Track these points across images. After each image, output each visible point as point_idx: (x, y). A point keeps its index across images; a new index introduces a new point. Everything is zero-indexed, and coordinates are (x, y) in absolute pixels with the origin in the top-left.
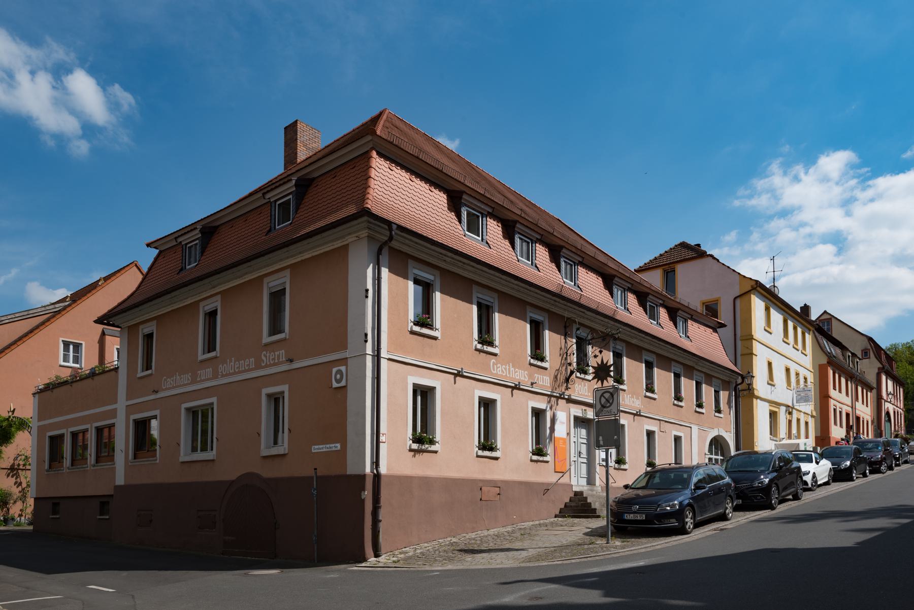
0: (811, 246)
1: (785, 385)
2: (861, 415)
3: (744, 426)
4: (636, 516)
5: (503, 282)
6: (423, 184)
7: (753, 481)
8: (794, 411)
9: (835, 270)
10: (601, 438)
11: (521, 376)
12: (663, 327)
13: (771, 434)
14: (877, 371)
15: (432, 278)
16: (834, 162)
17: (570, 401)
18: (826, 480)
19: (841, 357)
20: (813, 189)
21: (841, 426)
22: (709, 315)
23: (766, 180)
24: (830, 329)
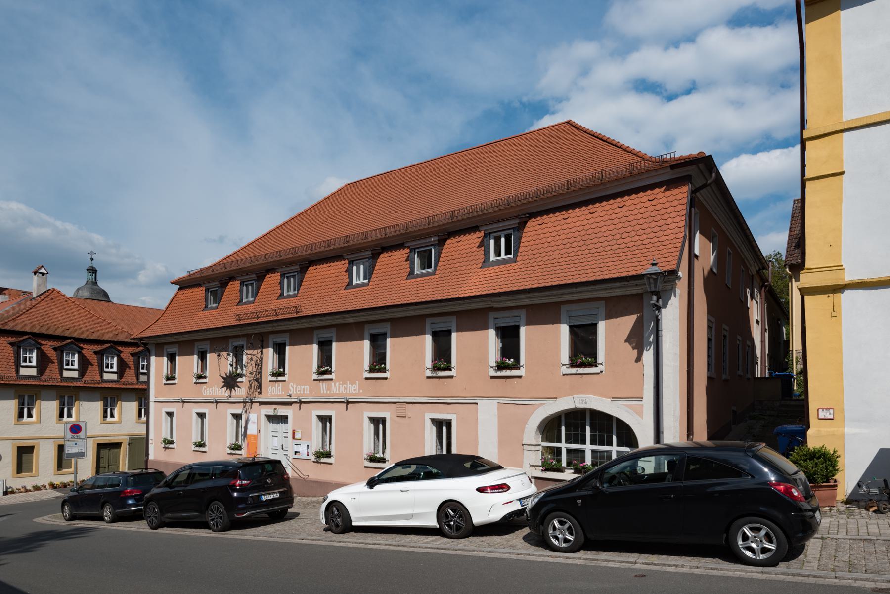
17: (261, 403)
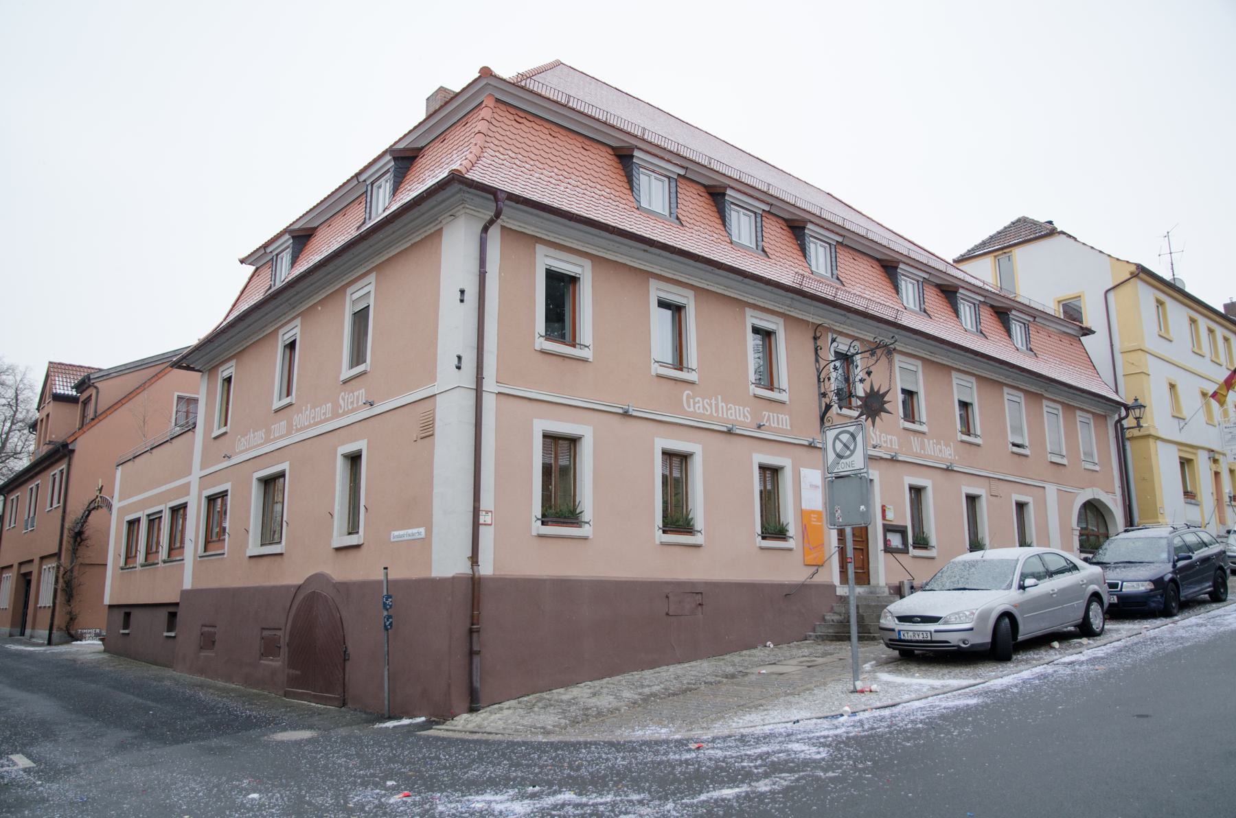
11: (739, 415)
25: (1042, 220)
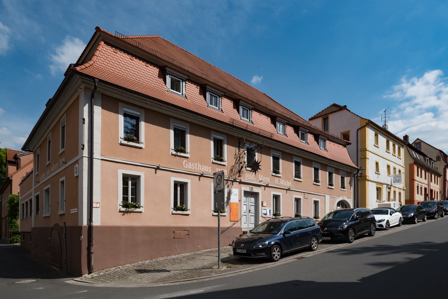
0: (421, 114)
1: (387, 174)
2: (434, 189)
3: (360, 196)
4: (248, 251)
5: (192, 117)
6: (141, 62)
7: (337, 227)
8: (392, 187)
9: (434, 124)
10: (217, 204)
12: (310, 144)
13: (378, 199)
14: (444, 167)
15: (139, 114)
16: (432, 76)
17: (241, 183)
18: (398, 223)
19: (423, 160)
20: (422, 88)
21: (421, 194)
22: (344, 140)
23: (399, 86)
24: (420, 147)
25: (343, 106)
